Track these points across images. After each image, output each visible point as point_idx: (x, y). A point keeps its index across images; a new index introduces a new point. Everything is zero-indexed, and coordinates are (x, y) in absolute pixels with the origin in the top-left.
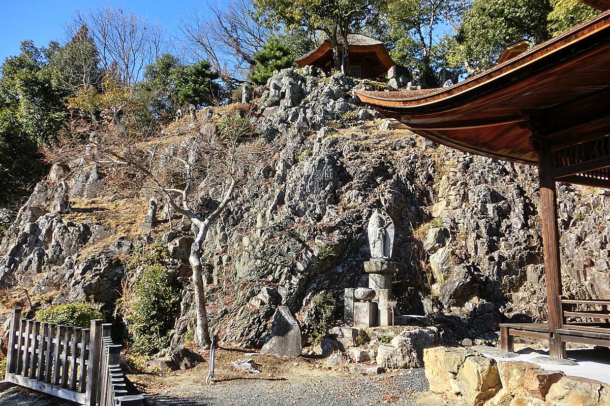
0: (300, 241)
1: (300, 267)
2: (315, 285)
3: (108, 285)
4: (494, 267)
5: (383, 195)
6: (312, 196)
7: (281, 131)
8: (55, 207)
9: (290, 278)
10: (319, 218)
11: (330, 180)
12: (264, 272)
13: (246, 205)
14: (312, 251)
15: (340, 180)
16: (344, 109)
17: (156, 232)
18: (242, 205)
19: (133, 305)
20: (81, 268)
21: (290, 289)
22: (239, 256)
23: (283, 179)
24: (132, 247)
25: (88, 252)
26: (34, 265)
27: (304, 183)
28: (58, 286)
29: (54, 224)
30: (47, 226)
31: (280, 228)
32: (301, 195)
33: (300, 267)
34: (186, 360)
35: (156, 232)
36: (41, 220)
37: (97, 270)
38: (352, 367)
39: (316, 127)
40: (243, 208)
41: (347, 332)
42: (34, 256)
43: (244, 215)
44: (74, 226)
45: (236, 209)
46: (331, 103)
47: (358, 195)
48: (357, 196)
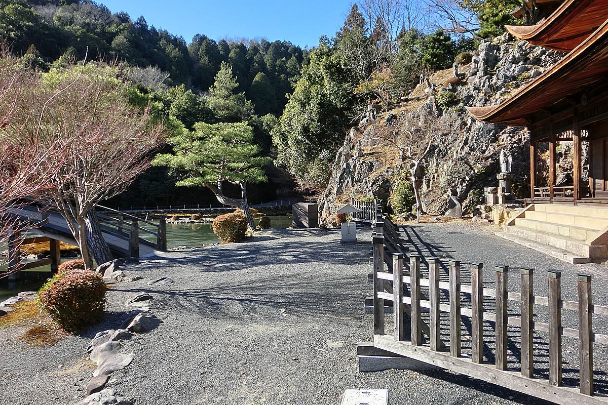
0: (470, 166)
1: (467, 178)
2: (475, 187)
3: (384, 191)
4: (586, 173)
5: (524, 135)
6: (482, 139)
7: (474, 96)
8: (355, 153)
9: (462, 184)
10: (484, 151)
11: (493, 129)
12: (450, 183)
13: (450, 146)
14: (474, 171)
15: (499, 128)
17: (404, 164)
19: (395, 200)
20: (371, 184)
21: (462, 189)
22: (442, 172)
23: (469, 129)
24: (393, 172)
25: (373, 176)
26: (350, 183)
28: (361, 193)
29: (356, 163)
30: (353, 164)
31: (462, 159)
33: (467, 178)
34: (411, 217)
35: (404, 164)
36: (350, 161)
37: (377, 184)
38: (472, 220)
39: (498, 88)
40: (448, 148)
41: (483, 207)
42: (349, 179)
44: (366, 163)
47: (508, 137)
48: (507, 138)
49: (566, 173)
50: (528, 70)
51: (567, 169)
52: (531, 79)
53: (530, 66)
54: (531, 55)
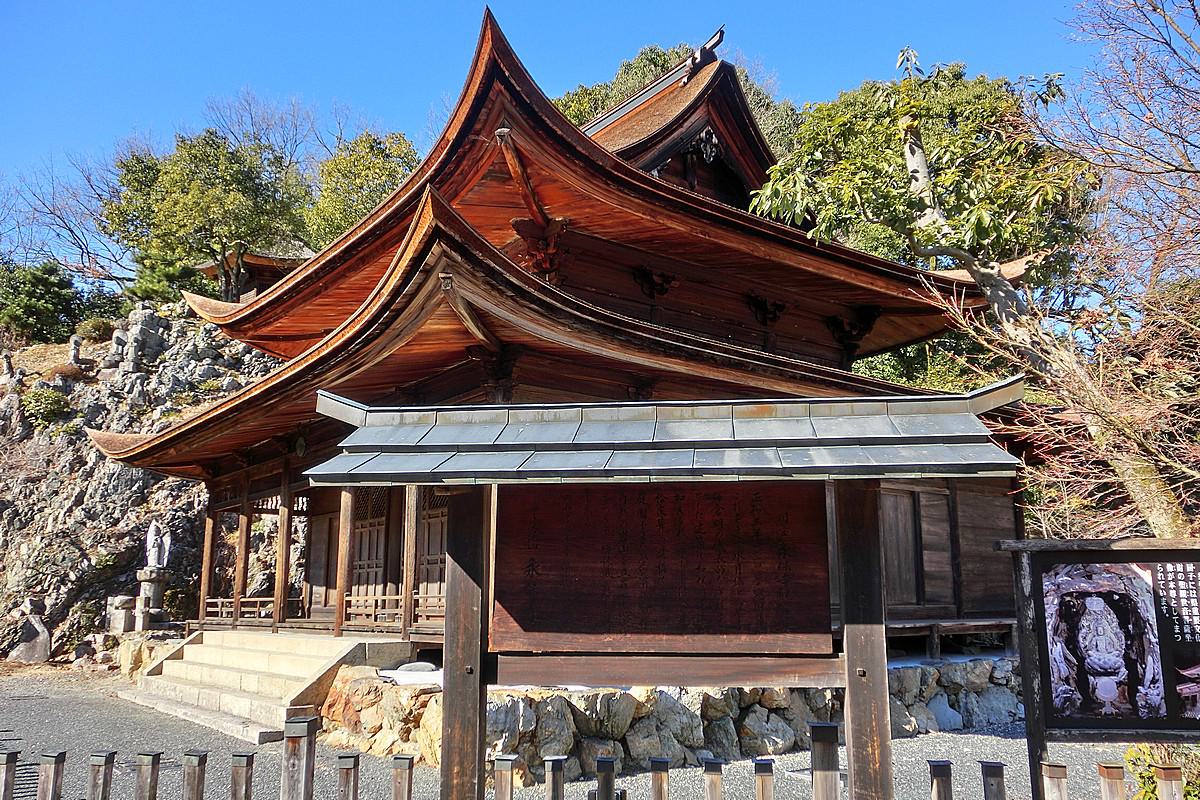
0: (81, 549)
1: (72, 577)
2: (87, 595)
5: (199, 496)
10: (117, 522)
11: (139, 479)
14: (89, 560)
15: (152, 478)
16: (206, 376)
18: (34, 504)
23: (90, 474)
27: (106, 482)
31: (65, 534)
32: (102, 495)
33: (72, 577)
39: (159, 401)
41: (100, 638)
43: (35, 517)
45: (26, 510)
46: (191, 367)
49: (267, 572)
50: (219, 375)
51: (271, 565)
52: (221, 394)
53: (222, 370)
54: (227, 350)
